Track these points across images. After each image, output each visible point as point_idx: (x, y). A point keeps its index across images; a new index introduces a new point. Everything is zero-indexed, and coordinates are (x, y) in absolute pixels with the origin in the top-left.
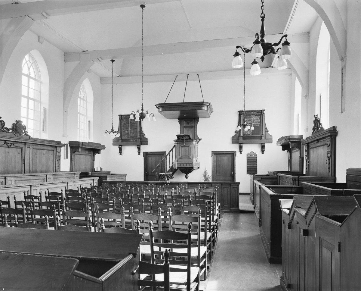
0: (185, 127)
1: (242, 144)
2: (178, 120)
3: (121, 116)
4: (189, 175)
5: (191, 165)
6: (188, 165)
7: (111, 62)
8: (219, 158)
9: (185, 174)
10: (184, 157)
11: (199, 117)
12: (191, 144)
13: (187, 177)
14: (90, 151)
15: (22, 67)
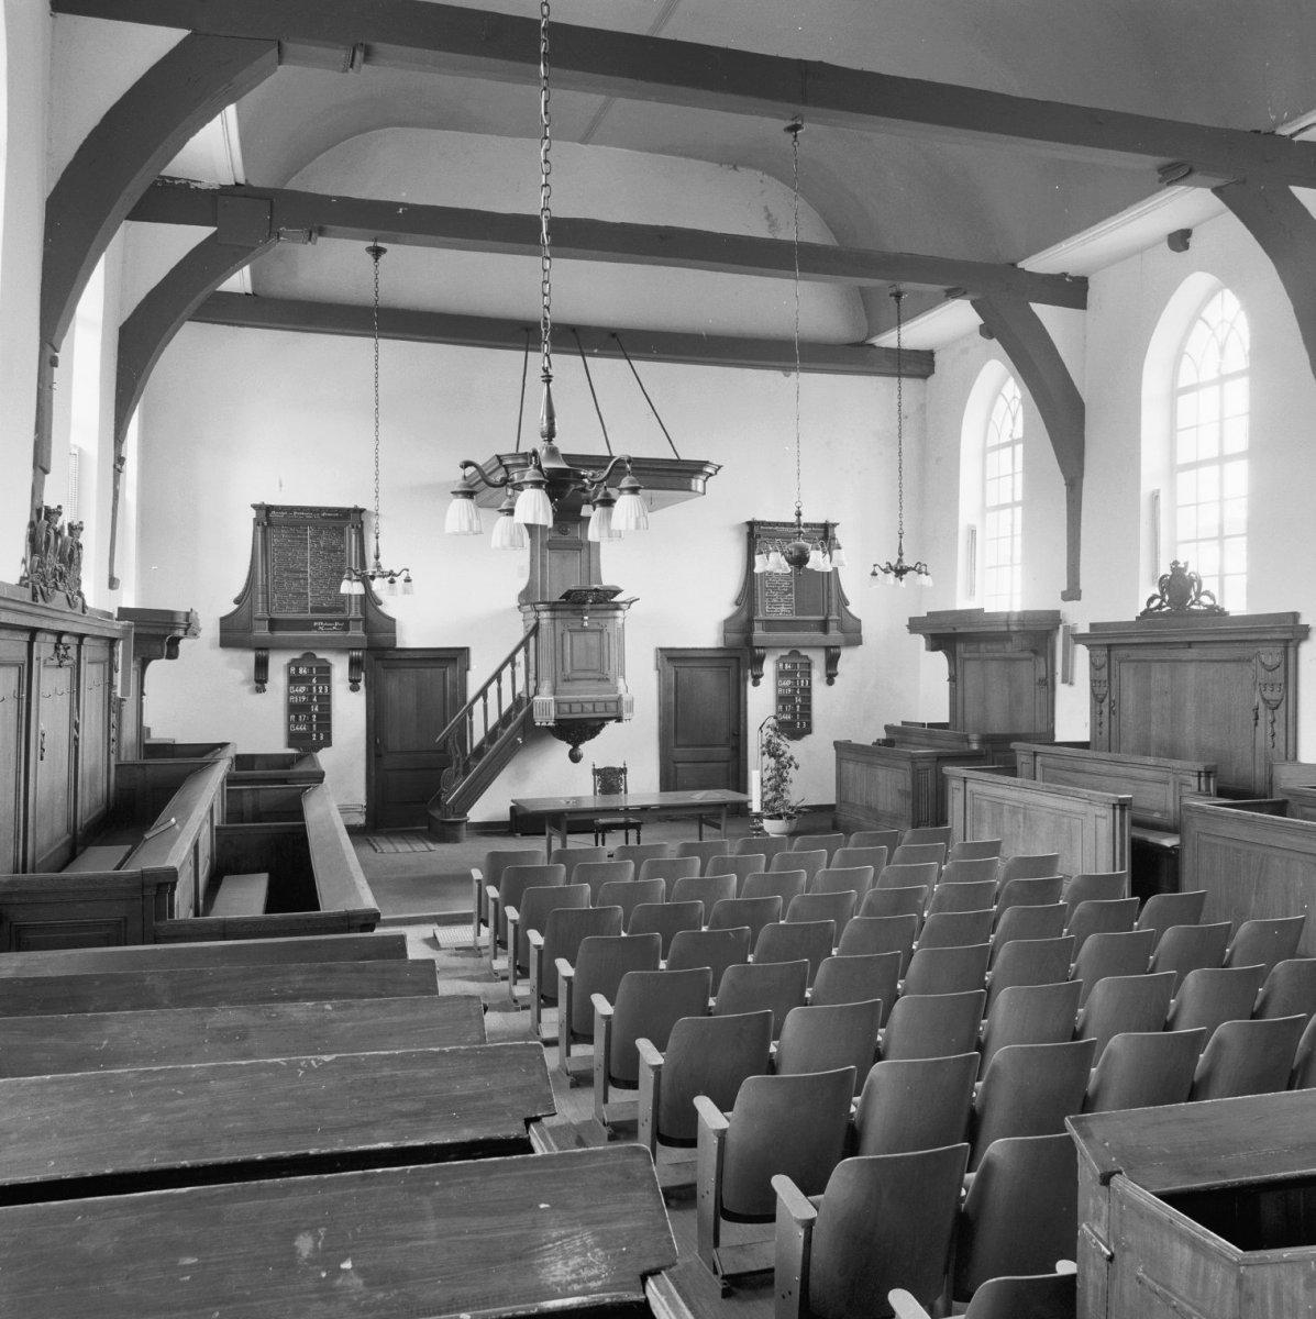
1: (266, 649)
3: (269, 509)
4: (586, 748)
5: (613, 706)
6: (576, 708)
7: (369, 257)
9: (568, 742)
12: (610, 620)
14: (743, 631)
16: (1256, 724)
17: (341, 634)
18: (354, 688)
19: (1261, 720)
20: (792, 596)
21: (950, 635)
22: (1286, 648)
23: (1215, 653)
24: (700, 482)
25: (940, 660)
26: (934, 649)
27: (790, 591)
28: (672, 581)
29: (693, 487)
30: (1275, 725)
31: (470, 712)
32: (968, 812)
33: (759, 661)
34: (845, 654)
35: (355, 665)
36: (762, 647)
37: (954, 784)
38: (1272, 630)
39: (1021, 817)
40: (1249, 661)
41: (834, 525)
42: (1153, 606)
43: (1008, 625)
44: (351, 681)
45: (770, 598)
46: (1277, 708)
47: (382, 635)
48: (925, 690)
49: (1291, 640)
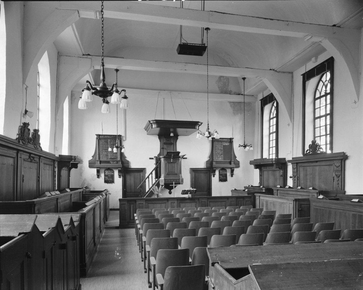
0: (165, 144)
2: (157, 137)
8: (197, 174)
10: (171, 173)
11: (179, 134)
13: (170, 193)
15: (275, 111)
16: (334, 181)
17: (116, 164)
18: (120, 177)
19: (335, 180)
20: (222, 156)
21: (260, 165)
22: (342, 161)
23: (323, 163)
24: (197, 127)
25: (257, 171)
26: (256, 168)
27: (222, 154)
28: (194, 152)
29: (196, 128)
30: (339, 181)
31: (145, 182)
32: (260, 204)
33: (214, 171)
34: (235, 169)
35: (119, 171)
36: (215, 168)
37: (257, 198)
38: (338, 157)
39: (272, 205)
40: (332, 165)
41: (233, 138)
42: (307, 152)
43: (272, 162)
44: (119, 175)
45: (217, 156)
46: (339, 177)
47: (126, 165)
48: (254, 178)
49: (343, 159)
